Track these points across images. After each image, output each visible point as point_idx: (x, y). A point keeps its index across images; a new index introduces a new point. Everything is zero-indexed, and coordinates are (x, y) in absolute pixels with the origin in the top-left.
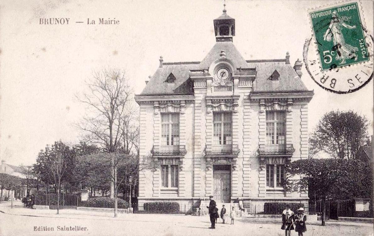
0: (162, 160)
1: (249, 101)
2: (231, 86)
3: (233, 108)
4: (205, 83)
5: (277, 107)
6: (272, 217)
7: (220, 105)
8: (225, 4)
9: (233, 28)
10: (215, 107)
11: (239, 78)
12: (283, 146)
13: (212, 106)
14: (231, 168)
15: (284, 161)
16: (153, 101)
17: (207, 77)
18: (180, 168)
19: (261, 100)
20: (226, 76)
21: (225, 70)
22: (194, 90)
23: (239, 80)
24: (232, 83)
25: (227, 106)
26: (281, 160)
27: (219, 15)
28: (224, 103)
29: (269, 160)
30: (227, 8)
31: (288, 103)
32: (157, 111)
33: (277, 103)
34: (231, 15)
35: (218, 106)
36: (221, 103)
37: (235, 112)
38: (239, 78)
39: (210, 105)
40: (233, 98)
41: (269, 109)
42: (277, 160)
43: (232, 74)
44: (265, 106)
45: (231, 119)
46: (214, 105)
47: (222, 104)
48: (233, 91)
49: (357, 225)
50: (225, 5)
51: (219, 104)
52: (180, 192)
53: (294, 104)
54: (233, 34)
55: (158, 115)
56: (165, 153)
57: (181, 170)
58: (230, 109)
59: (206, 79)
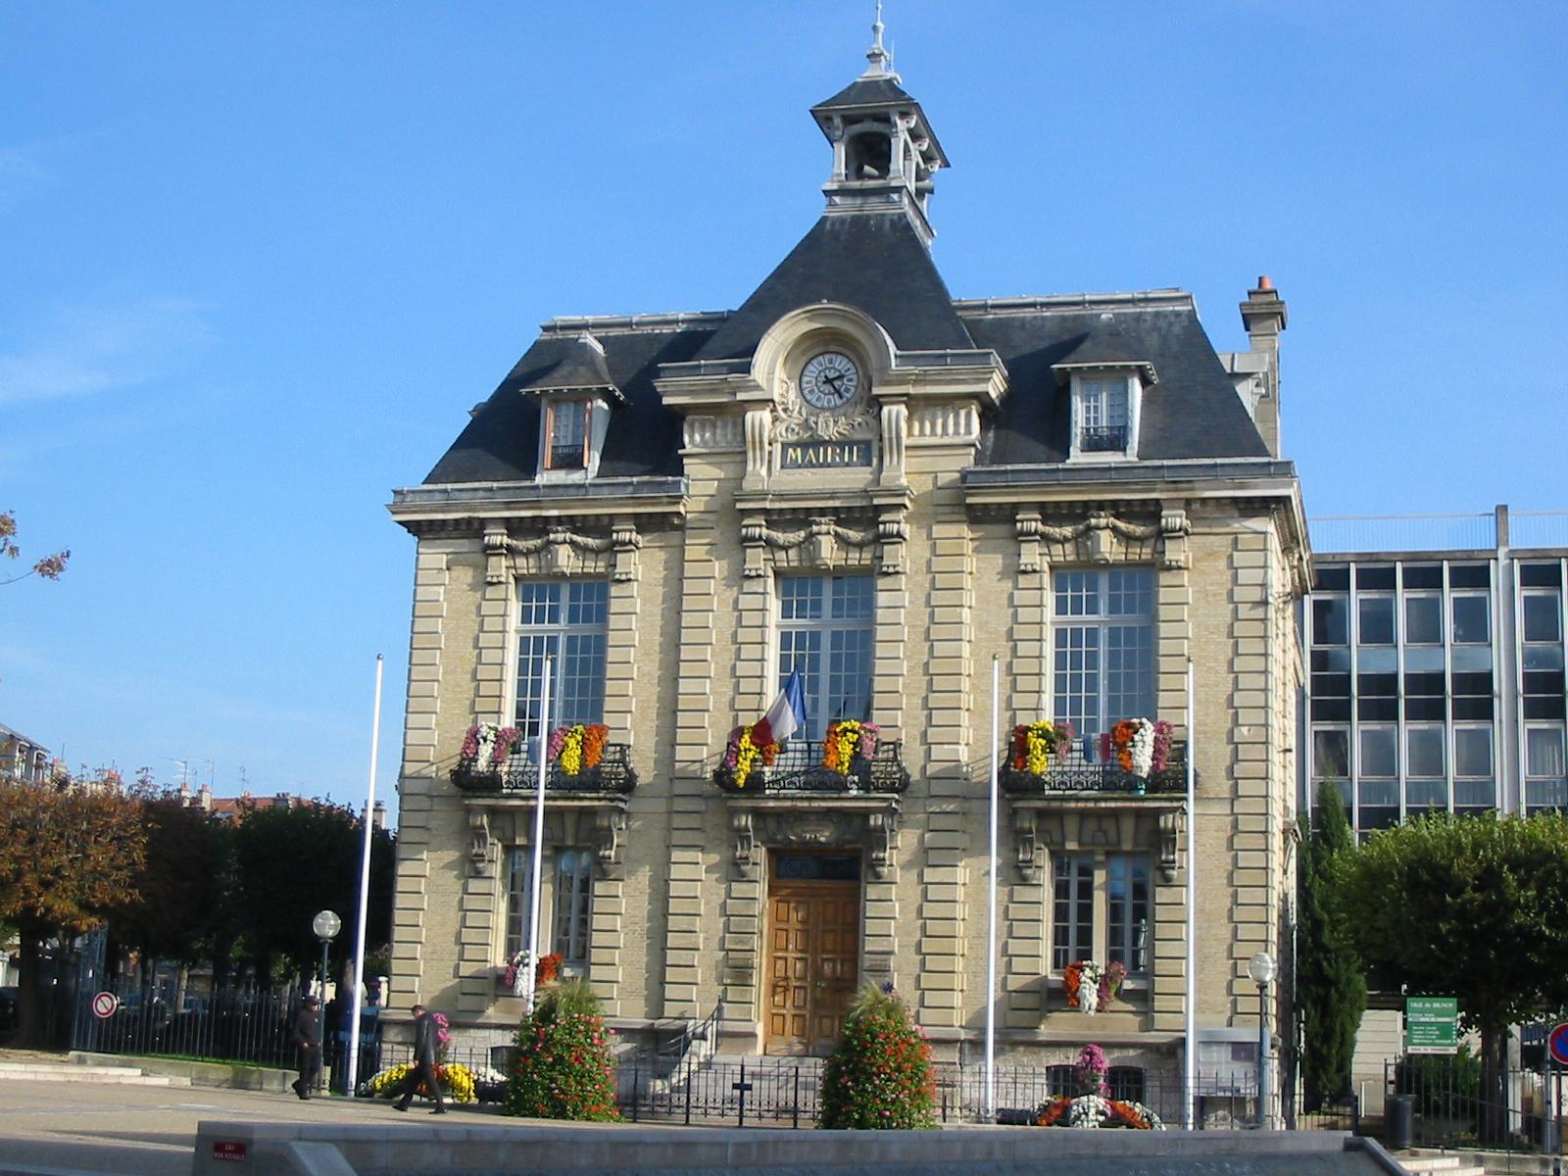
3: (1159, 548)
5: (566, 560)
7: (812, 535)
10: (785, 548)
11: (910, 401)
12: (798, 755)
13: (770, 544)
17: (741, 396)
20: (812, 392)
21: (841, 364)
22: (685, 461)
25: (843, 542)
29: (516, 819)
31: (615, 536)
33: (1107, 527)
35: (799, 545)
37: (887, 574)
38: (910, 401)
39: (1036, 532)
40: (876, 501)
42: (1109, 825)
44: (1046, 539)
45: (869, 606)
46: (780, 537)
47: (1098, 528)
48: (875, 461)
49: (118, 1141)
51: (802, 534)
52: (1159, 1003)
57: (878, 876)
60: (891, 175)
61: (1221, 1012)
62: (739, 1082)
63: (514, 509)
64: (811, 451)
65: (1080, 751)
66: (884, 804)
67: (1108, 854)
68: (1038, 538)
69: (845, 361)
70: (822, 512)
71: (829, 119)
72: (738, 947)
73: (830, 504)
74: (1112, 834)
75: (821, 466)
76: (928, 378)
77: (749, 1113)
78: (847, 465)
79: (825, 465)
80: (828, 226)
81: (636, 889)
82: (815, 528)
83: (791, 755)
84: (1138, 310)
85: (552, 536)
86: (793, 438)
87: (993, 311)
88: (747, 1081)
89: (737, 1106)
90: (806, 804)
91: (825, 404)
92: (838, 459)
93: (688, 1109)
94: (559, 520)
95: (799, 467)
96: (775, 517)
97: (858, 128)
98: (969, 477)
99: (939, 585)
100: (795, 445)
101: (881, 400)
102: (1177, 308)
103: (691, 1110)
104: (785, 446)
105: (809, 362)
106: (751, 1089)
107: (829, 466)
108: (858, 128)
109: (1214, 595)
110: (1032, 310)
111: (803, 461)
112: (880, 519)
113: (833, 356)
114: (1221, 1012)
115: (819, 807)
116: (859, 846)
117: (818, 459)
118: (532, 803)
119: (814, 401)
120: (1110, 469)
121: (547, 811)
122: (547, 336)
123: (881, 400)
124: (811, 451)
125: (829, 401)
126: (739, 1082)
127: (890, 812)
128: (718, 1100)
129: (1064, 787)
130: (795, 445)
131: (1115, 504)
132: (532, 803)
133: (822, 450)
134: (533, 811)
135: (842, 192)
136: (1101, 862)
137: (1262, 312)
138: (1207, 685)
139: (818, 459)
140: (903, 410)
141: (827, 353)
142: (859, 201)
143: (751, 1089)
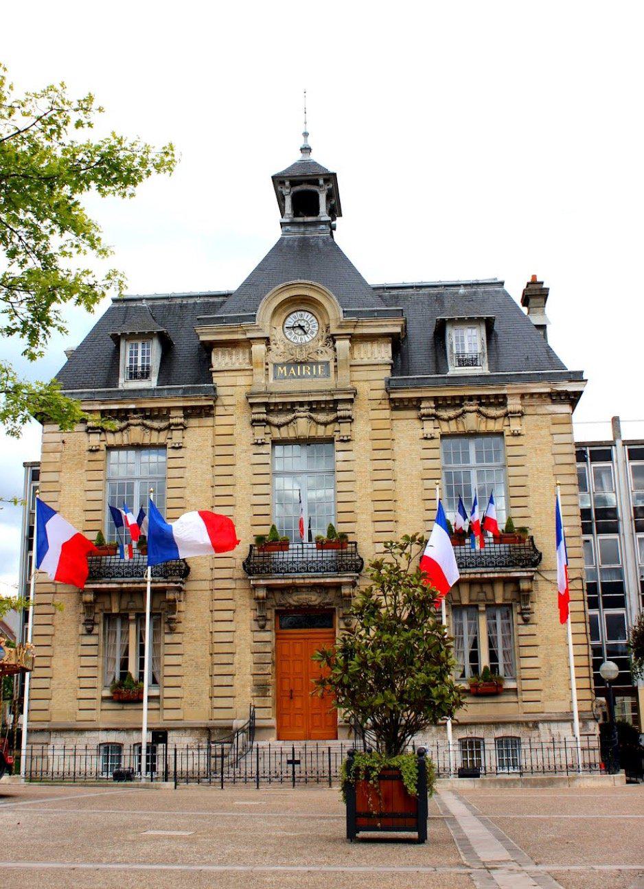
0: (110, 597)
1: (433, 405)
2: (328, 363)
4: (247, 356)
6: (15, 802)
8: (308, 131)
9: (333, 195)
14: (337, 619)
15: (508, 595)
16: (166, 407)
18: (171, 621)
19: (172, 412)
22: (214, 375)
23: (351, 341)
24: (331, 351)
26: (499, 590)
27: (286, 159)
28: (307, 414)
30: (311, 142)
32: (429, 427)
34: (325, 159)
36: (131, 421)
41: (158, 438)
42: (487, 589)
43: (328, 327)
46: (107, 426)
50: (306, 134)
53: (529, 410)
54: (335, 211)
55: (98, 453)
56: (292, 568)
58: (325, 432)
59: (249, 342)
60: (321, 214)
61: (564, 700)
62: (291, 759)
63: (107, 404)
64: (292, 369)
65: (469, 544)
66: (351, 580)
67: (487, 606)
68: (433, 418)
69: (310, 315)
70: (301, 404)
71: (282, 183)
72: (260, 672)
73: (306, 399)
74: (490, 596)
75: (299, 377)
76: (364, 324)
77: (227, 780)
78: (315, 376)
79: (302, 377)
80: (285, 243)
81: (191, 638)
82: (298, 414)
83: (290, 552)
84: (473, 290)
85: (131, 421)
86: (281, 360)
87: (388, 291)
88: (297, 758)
89: (219, 775)
90: (302, 581)
91: (299, 341)
92: (309, 373)
93: (258, 780)
94: (135, 411)
95: (285, 378)
96: (272, 408)
97: (298, 188)
98: (391, 382)
99: (384, 447)
100: (283, 365)
101: (335, 337)
102: (496, 289)
103: (332, 779)
104: (275, 365)
105: (288, 316)
106: (299, 763)
107: (304, 377)
108: (298, 188)
109: (540, 450)
110: (410, 290)
111: (288, 374)
112: (421, 406)
113: (303, 313)
114: (564, 700)
115: (310, 583)
116: (334, 607)
117: (297, 374)
118: (142, 585)
119: (292, 340)
120: (477, 376)
121: (153, 591)
122: (117, 305)
123: (335, 337)
124: (292, 369)
125: (301, 339)
126: (291, 759)
127: (180, 590)
128: (267, 771)
129: (323, 570)
130: (283, 365)
131: (479, 397)
132: (142, 585)
133: (314, 367)
134: (145, 589)
135: (291, 224)
136: (483, 611)
137: (536, 294)
138: (540, 503)
139: (297, 374)
140: (347, 343)
141: (300, 311)
142: (302, 229)
143: (299, 763)
